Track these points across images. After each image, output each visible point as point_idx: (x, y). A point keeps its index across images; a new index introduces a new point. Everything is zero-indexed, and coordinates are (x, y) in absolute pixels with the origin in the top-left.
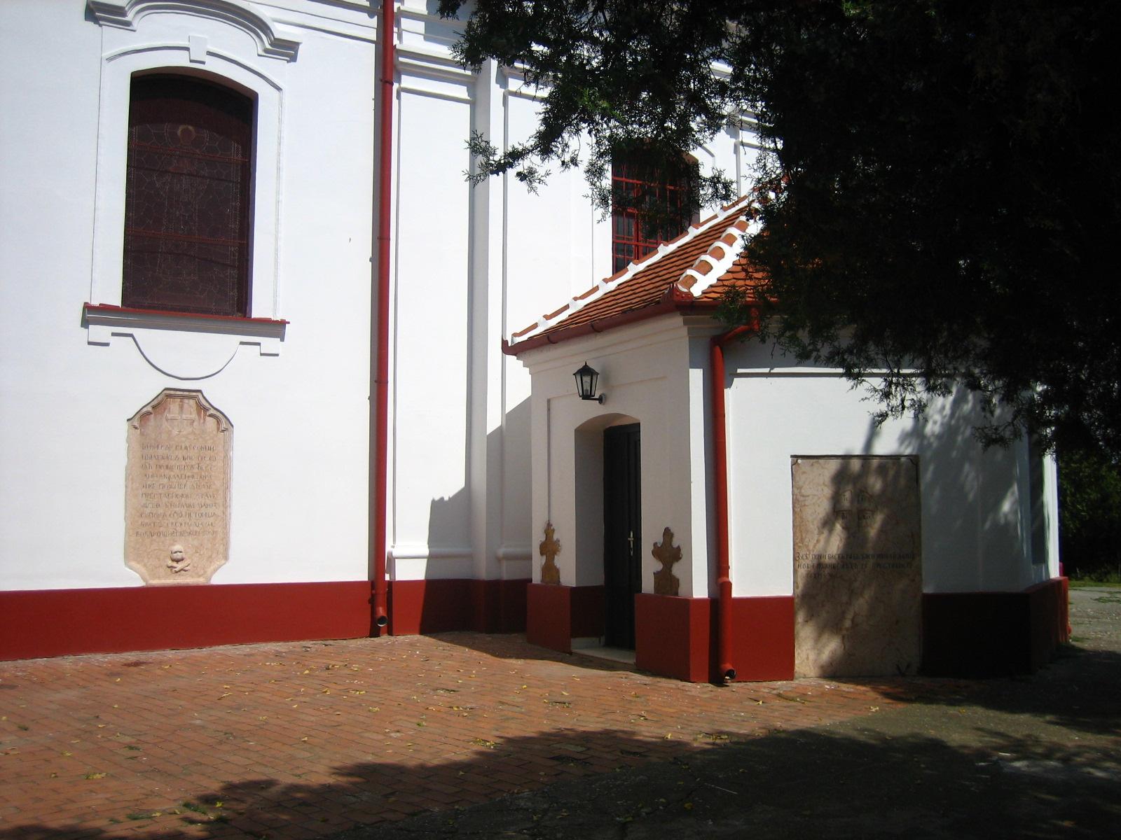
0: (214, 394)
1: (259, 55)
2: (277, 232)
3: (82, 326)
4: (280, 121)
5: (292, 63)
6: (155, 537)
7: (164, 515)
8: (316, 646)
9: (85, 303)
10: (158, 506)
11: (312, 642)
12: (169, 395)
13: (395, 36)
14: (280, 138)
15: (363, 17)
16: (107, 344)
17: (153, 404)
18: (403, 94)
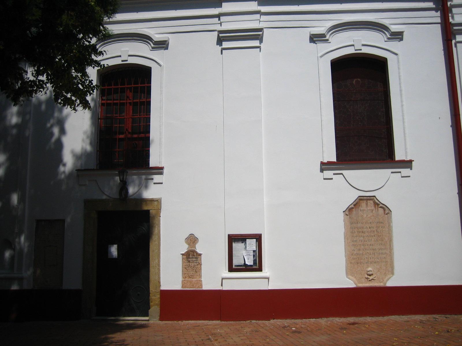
0: (382, 197)
1: (385, 41)
2: (403, 119)
3: (320, 172)
4: (399, 68)
5: (401, 42)
6: (359, 264)
7: (363, 254)
8: (441, 318)
9: (321, 162)
10: (359, 250)
11: (438, 316)
12: (361, 199)
13: (450, 18)
14: (400, 76)
15: (433, 13)
16: (332, 179)
17: (354, 204)
18: (458, 45)
